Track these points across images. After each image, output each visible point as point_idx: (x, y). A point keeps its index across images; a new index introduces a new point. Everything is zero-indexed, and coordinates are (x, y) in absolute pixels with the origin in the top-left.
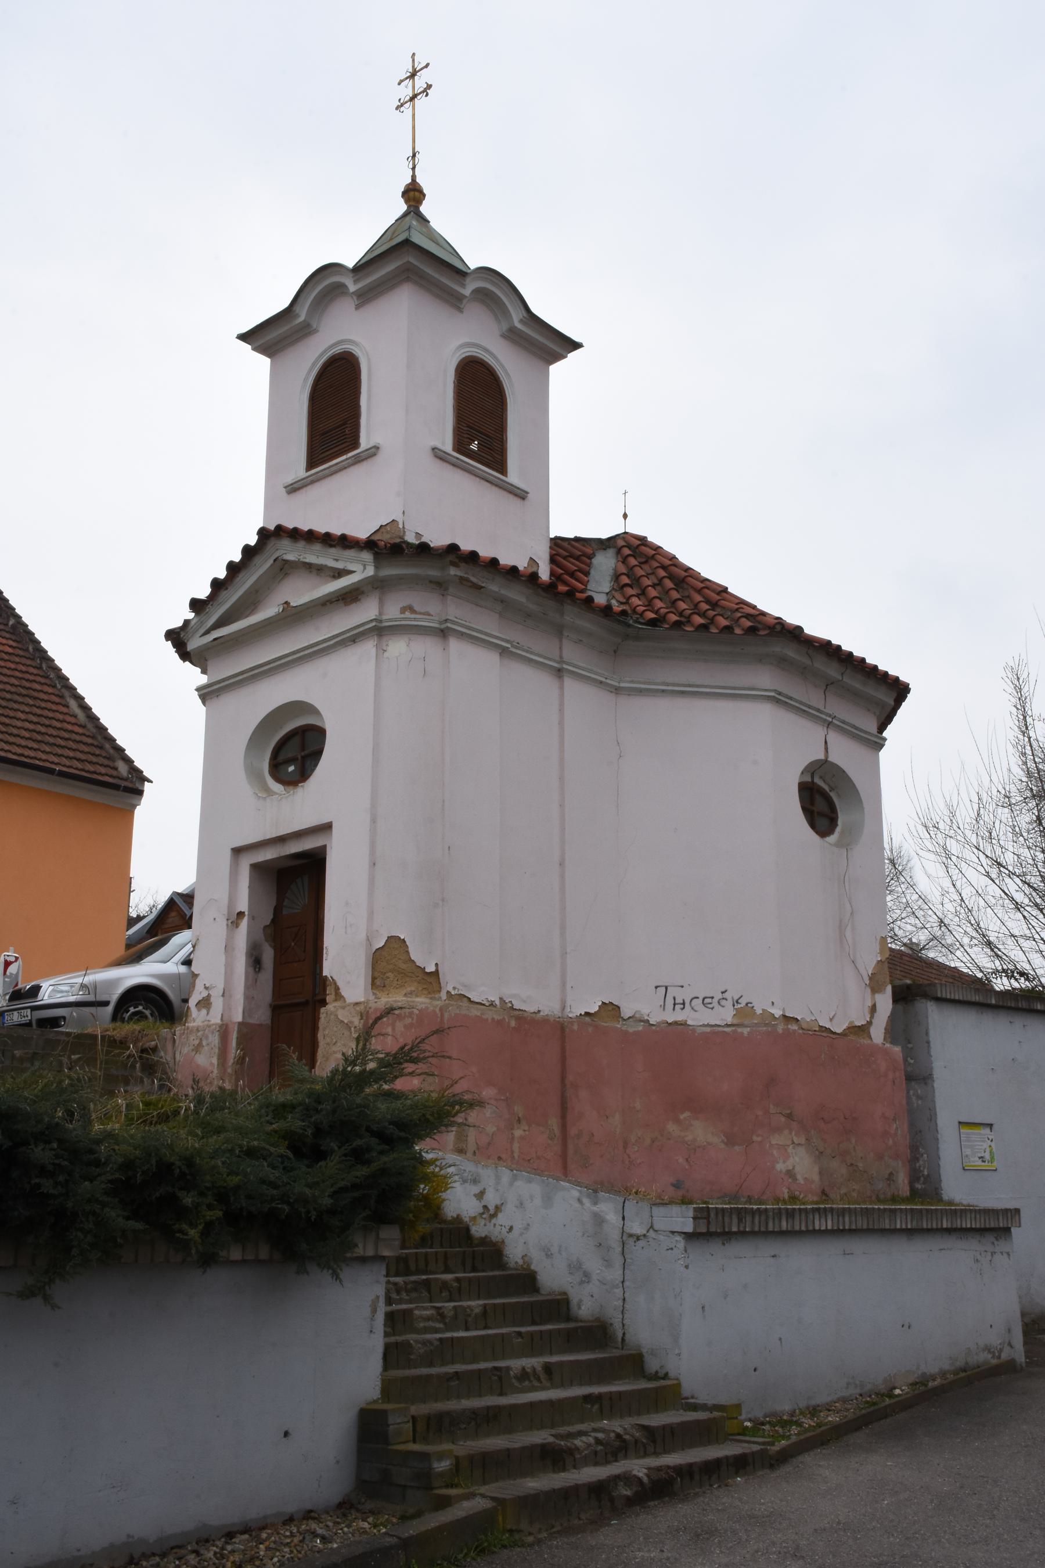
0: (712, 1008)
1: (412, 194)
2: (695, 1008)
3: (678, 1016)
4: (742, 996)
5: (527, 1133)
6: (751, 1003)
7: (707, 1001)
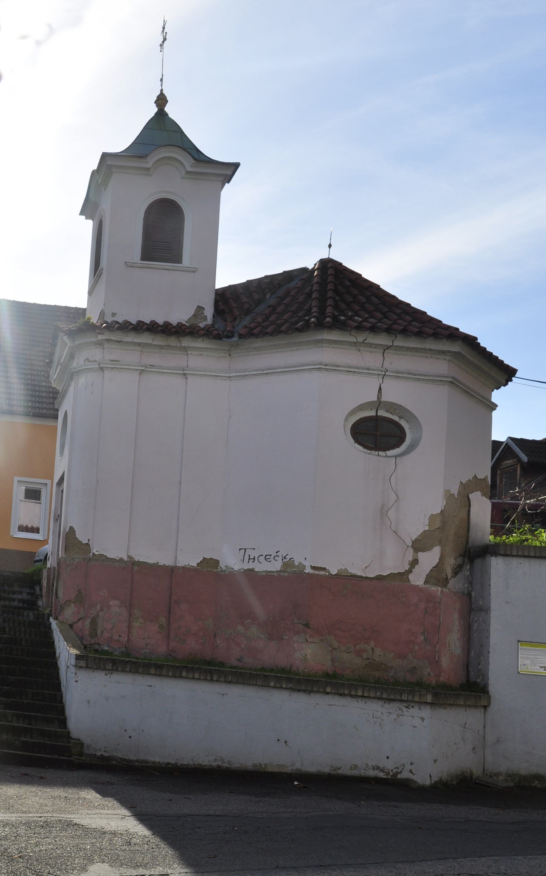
0: (270, 562)
1: (160, 101)
2: (260, 561)
3: (251, 566)
4: (288, 554)
5: (143, 625)
6: (293, 558)
7: (267, 557)
